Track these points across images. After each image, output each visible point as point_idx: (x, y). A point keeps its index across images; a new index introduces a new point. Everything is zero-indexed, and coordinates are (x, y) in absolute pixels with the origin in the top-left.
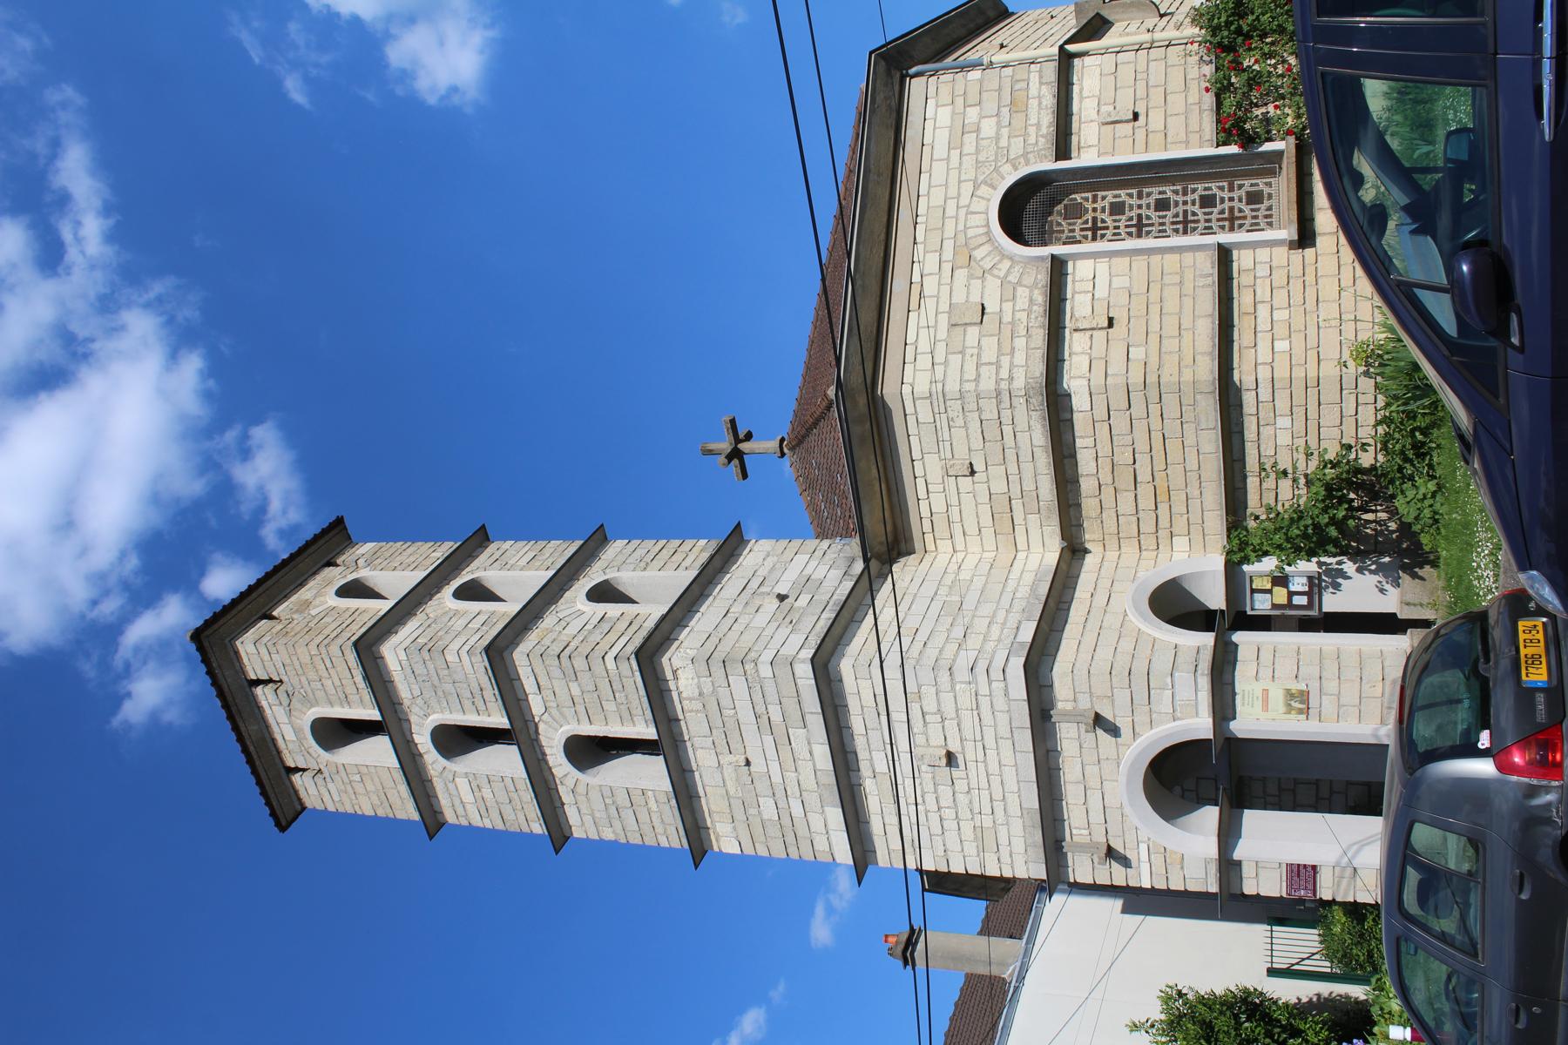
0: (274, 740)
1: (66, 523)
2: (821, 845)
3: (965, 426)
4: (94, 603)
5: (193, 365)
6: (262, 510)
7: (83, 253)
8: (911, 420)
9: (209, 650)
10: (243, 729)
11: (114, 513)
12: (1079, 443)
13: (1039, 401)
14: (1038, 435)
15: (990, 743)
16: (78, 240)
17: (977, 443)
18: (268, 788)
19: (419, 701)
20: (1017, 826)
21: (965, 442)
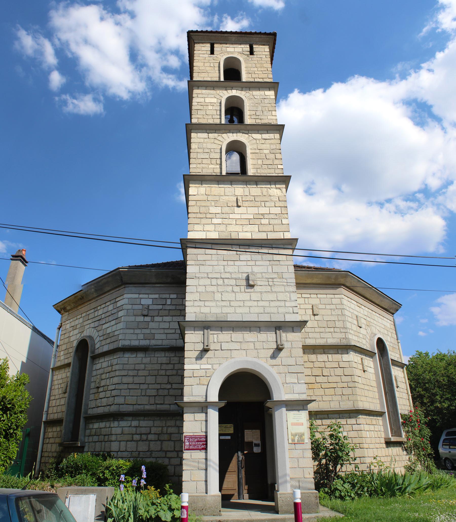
0: (226, 44)
1: (86, 42)
2: (197, 227)
3: (332, 315)
4: (59, 39)
5: (125, 96)
6: (75, 98)
7: (165, 78)
8: (332, 296)
9: (268, 36)
10: (235, 35)
11: (87, 56)
12: (330, 356)
13: (344, 342)
14: (332, 341)
15: (261, 304)
16: (168, 79)
17: (326, 318)
18: (208, 34)
19: (252, 97)
20: (218, 311)
21: (325, 314)
